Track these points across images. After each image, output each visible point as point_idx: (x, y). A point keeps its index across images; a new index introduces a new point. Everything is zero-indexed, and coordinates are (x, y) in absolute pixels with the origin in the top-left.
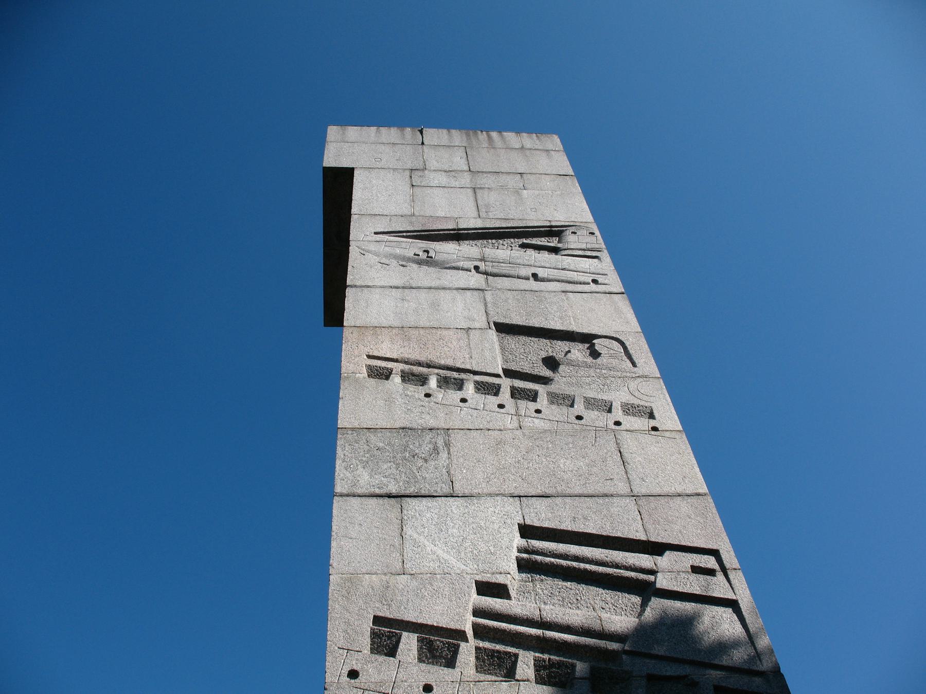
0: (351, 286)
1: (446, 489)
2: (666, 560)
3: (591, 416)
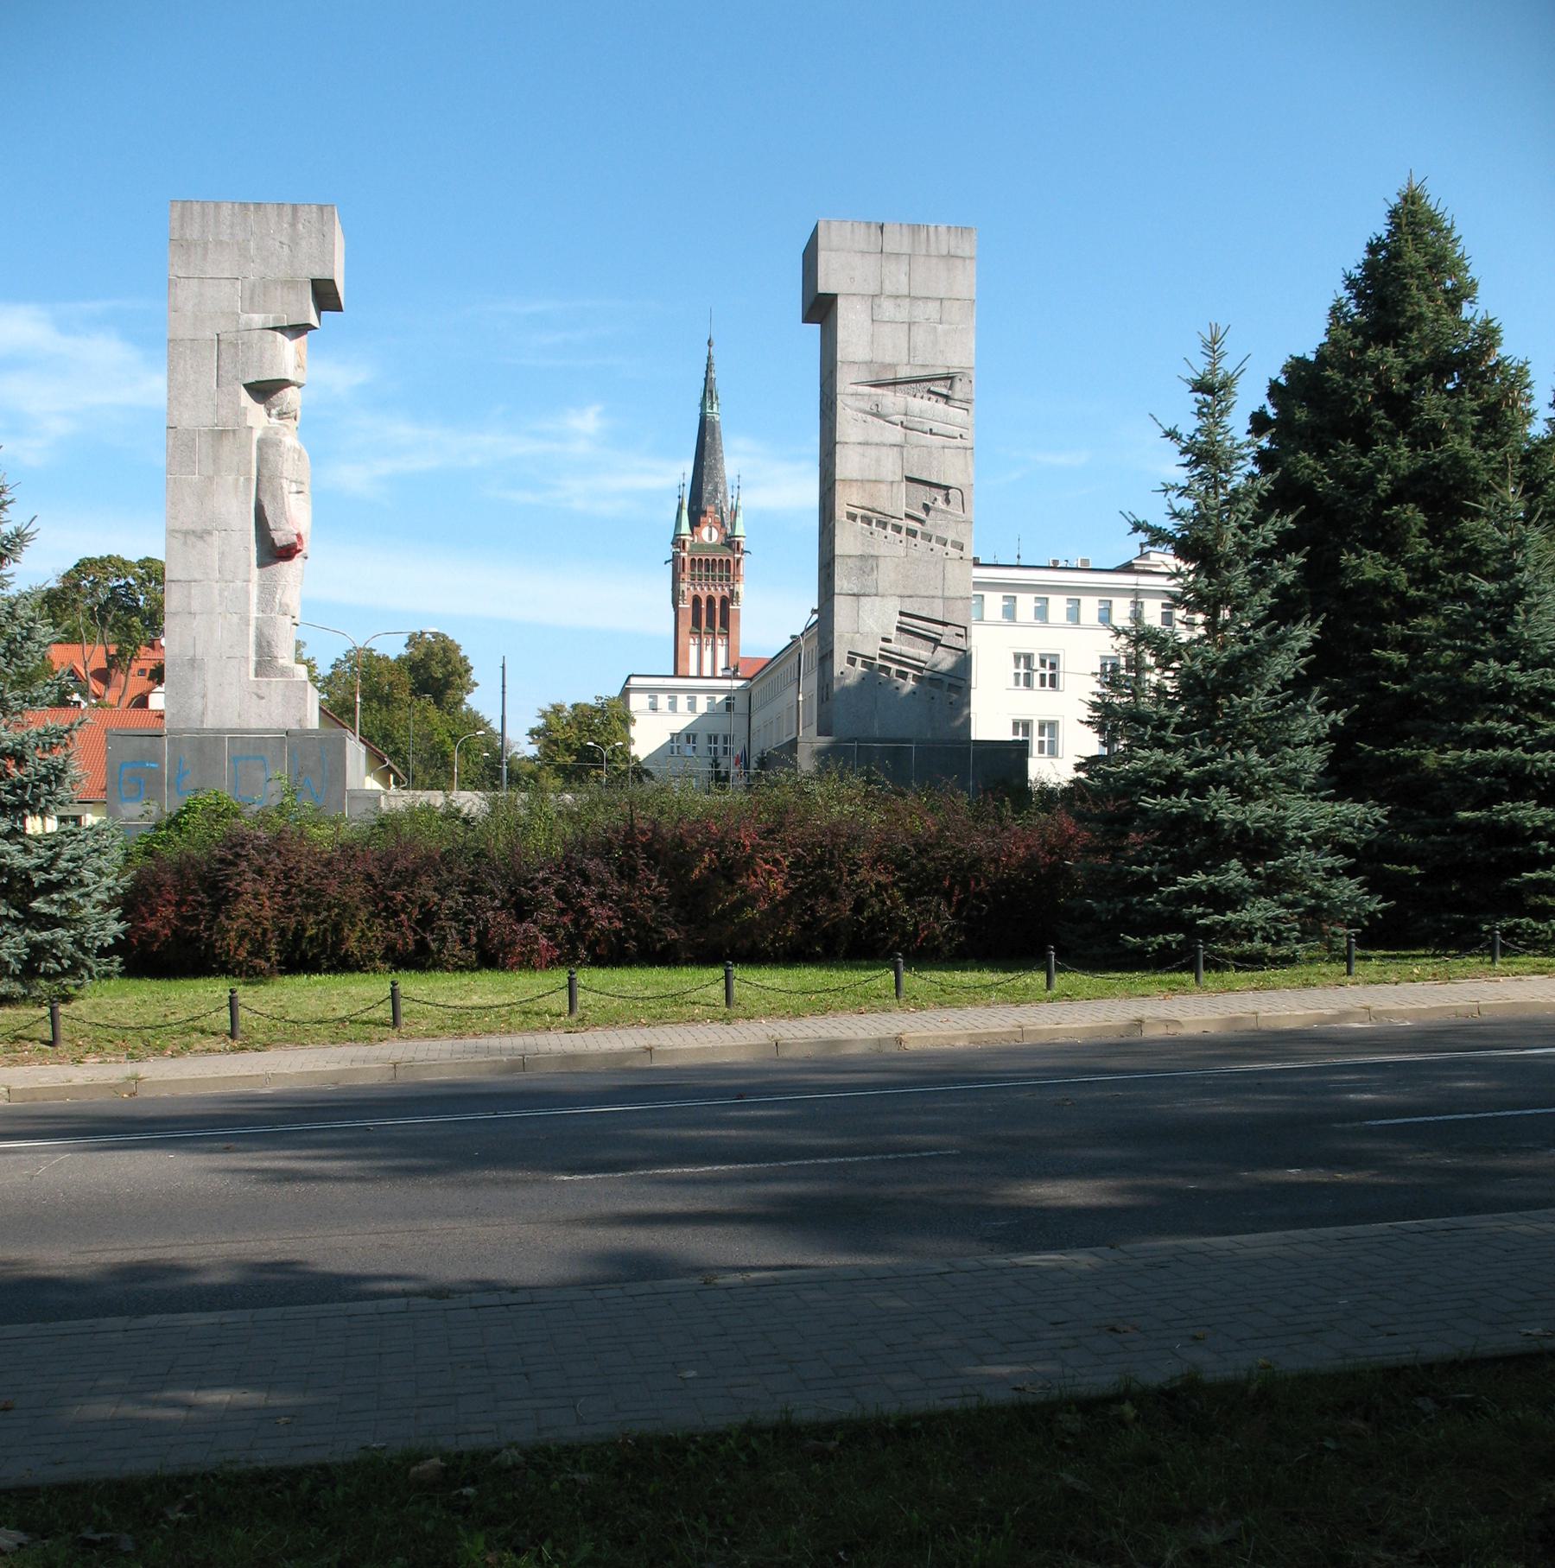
0: (728, 978)
1: (874, 591)
2: (947, 630)
3: (937, 546)
